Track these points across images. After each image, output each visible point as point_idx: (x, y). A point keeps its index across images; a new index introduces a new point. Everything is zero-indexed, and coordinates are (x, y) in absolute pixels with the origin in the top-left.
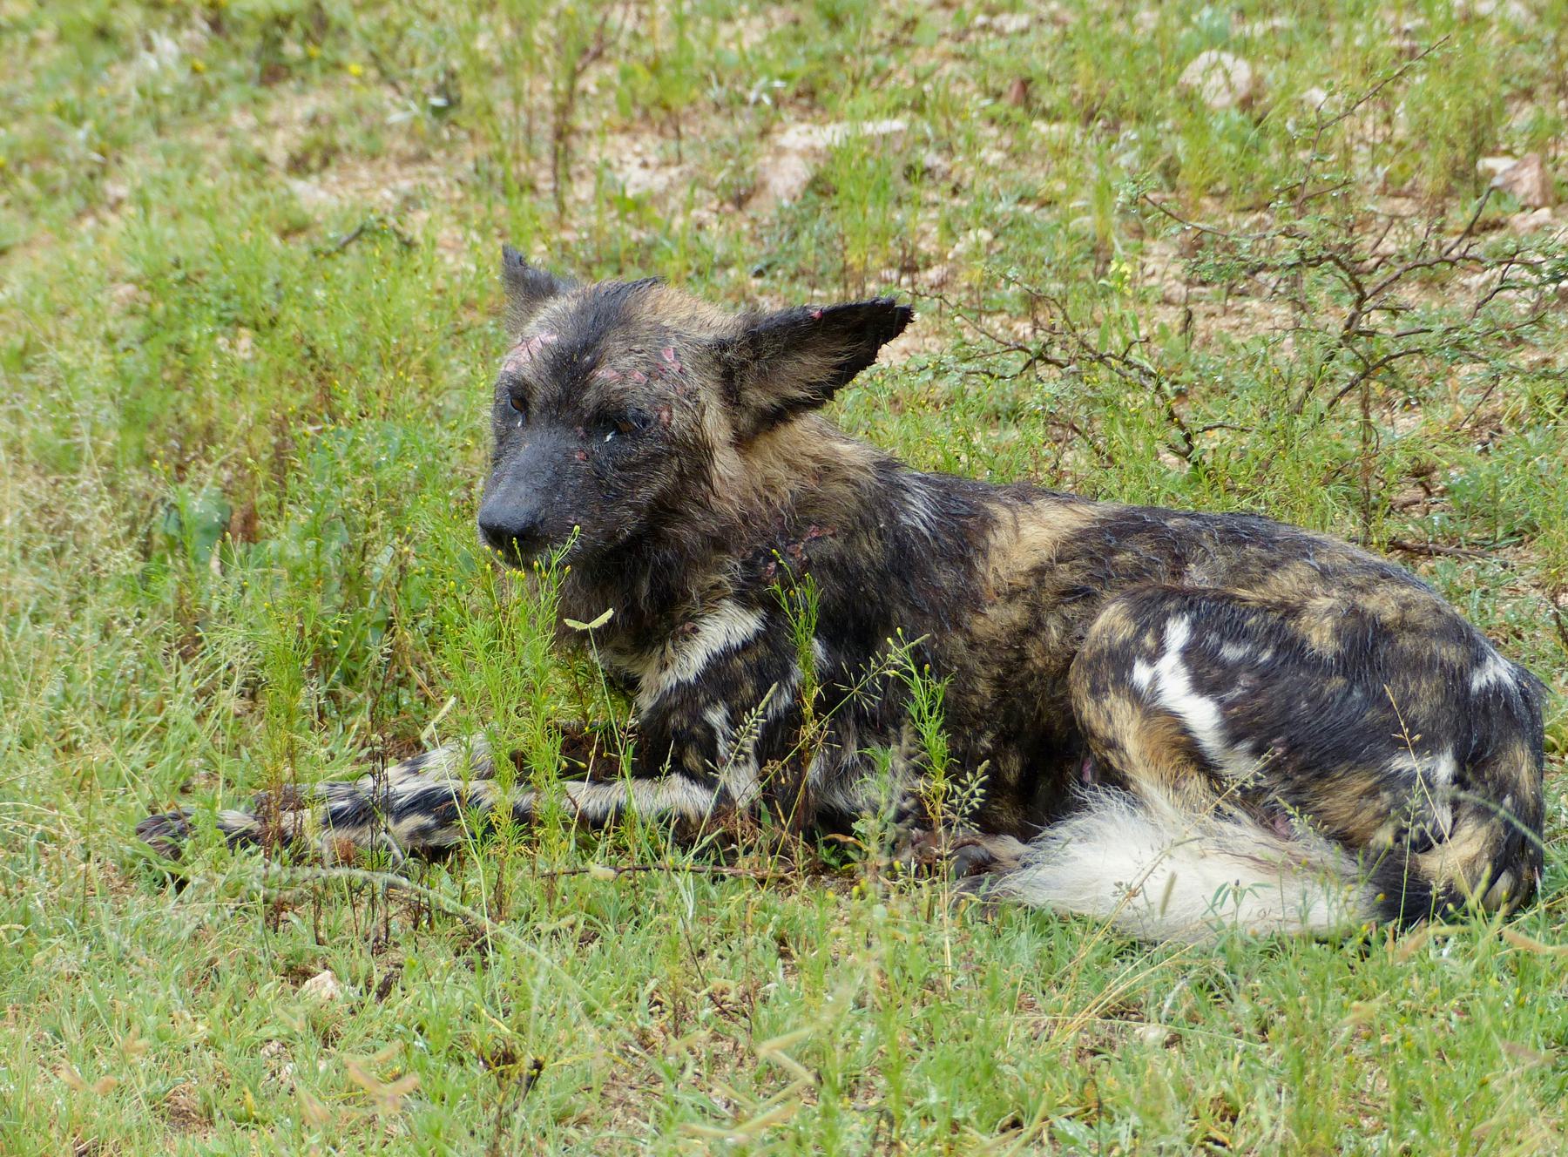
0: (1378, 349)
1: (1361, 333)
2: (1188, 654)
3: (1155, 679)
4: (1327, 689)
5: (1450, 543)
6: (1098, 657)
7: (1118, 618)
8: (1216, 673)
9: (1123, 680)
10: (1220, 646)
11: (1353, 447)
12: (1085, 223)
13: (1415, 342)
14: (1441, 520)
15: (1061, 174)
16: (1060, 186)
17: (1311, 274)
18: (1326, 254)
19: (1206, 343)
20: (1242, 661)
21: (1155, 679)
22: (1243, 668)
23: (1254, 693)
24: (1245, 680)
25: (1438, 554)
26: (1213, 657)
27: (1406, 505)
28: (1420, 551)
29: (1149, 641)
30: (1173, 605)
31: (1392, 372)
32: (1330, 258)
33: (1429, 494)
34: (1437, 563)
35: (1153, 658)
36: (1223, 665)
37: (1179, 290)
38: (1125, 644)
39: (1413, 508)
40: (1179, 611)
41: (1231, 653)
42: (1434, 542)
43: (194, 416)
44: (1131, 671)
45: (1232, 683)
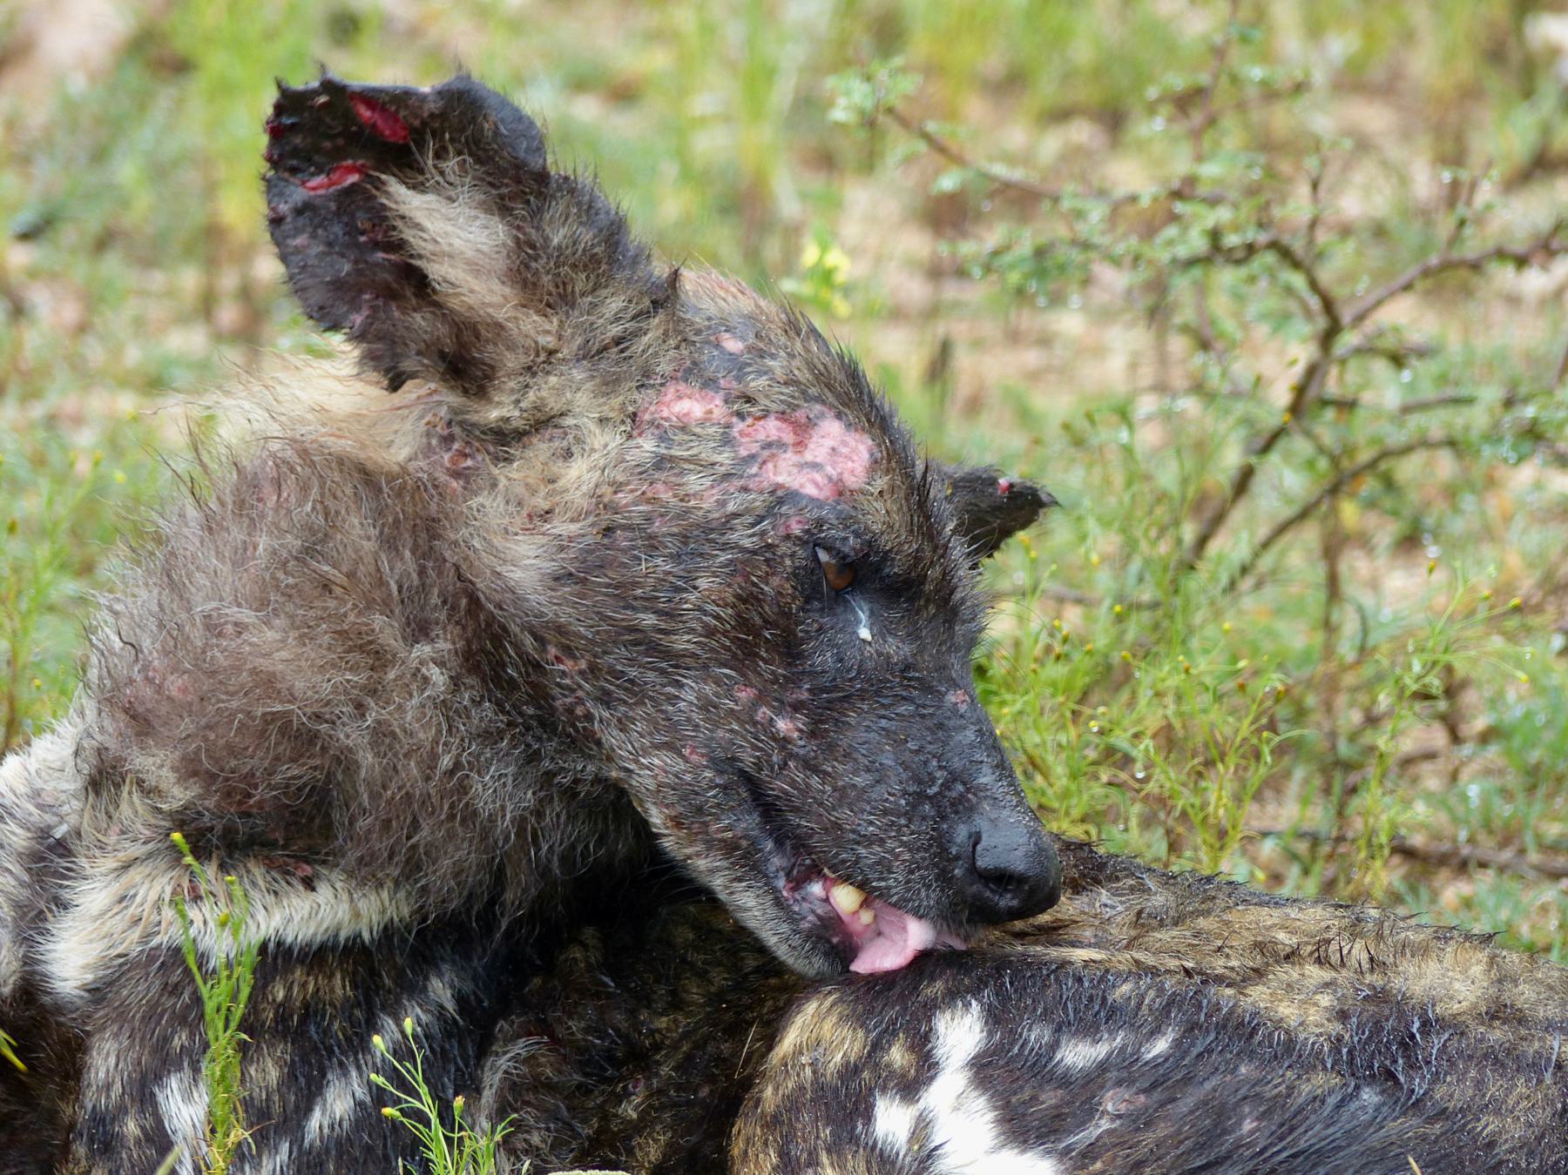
0: (1365, 432)
1: (1325, 403)
2: (984, 1070)
3: (922, 1127)
4: (1305, 1088)
5: (1505, 842)
6: (793, 1104)
7: (828, 1025)
8: (1050, 1098)
9: (854, 1139)
10: (1054, 1046)
11: (1298, 637)
12: (710, 145)
13: (1435, 423)
14: (1485, 798)
15: (656, 36)
16: (657, 61)
17: (1226, 276)
18: (1263, 238)
19: (974, 406)
20: (1103, 1067)
21: (922, 1127)
22: (1113, 1075)
23: (1138, 1121)
24: (1113, 1102)
25: (1483, 865)
26: (1040, 1068)
27: (1408, 762)
28: (1443, 860)
29: (897, 1055)
30: (939, 985)
31: (1389, 483)
32: (1274, 245)
33: (1456, 738)
34: (1481, 884)
35: (910, 1087)
36: (1065, 1080)
37: (916, 290)
38: (850, 1071)
39: (1426, 768)
40: (953, 996)
41: (1078, 1054)
42: (1471, 840)
43: (685, 1049)
44: (868, 1116)
45: (1090, 1111)
